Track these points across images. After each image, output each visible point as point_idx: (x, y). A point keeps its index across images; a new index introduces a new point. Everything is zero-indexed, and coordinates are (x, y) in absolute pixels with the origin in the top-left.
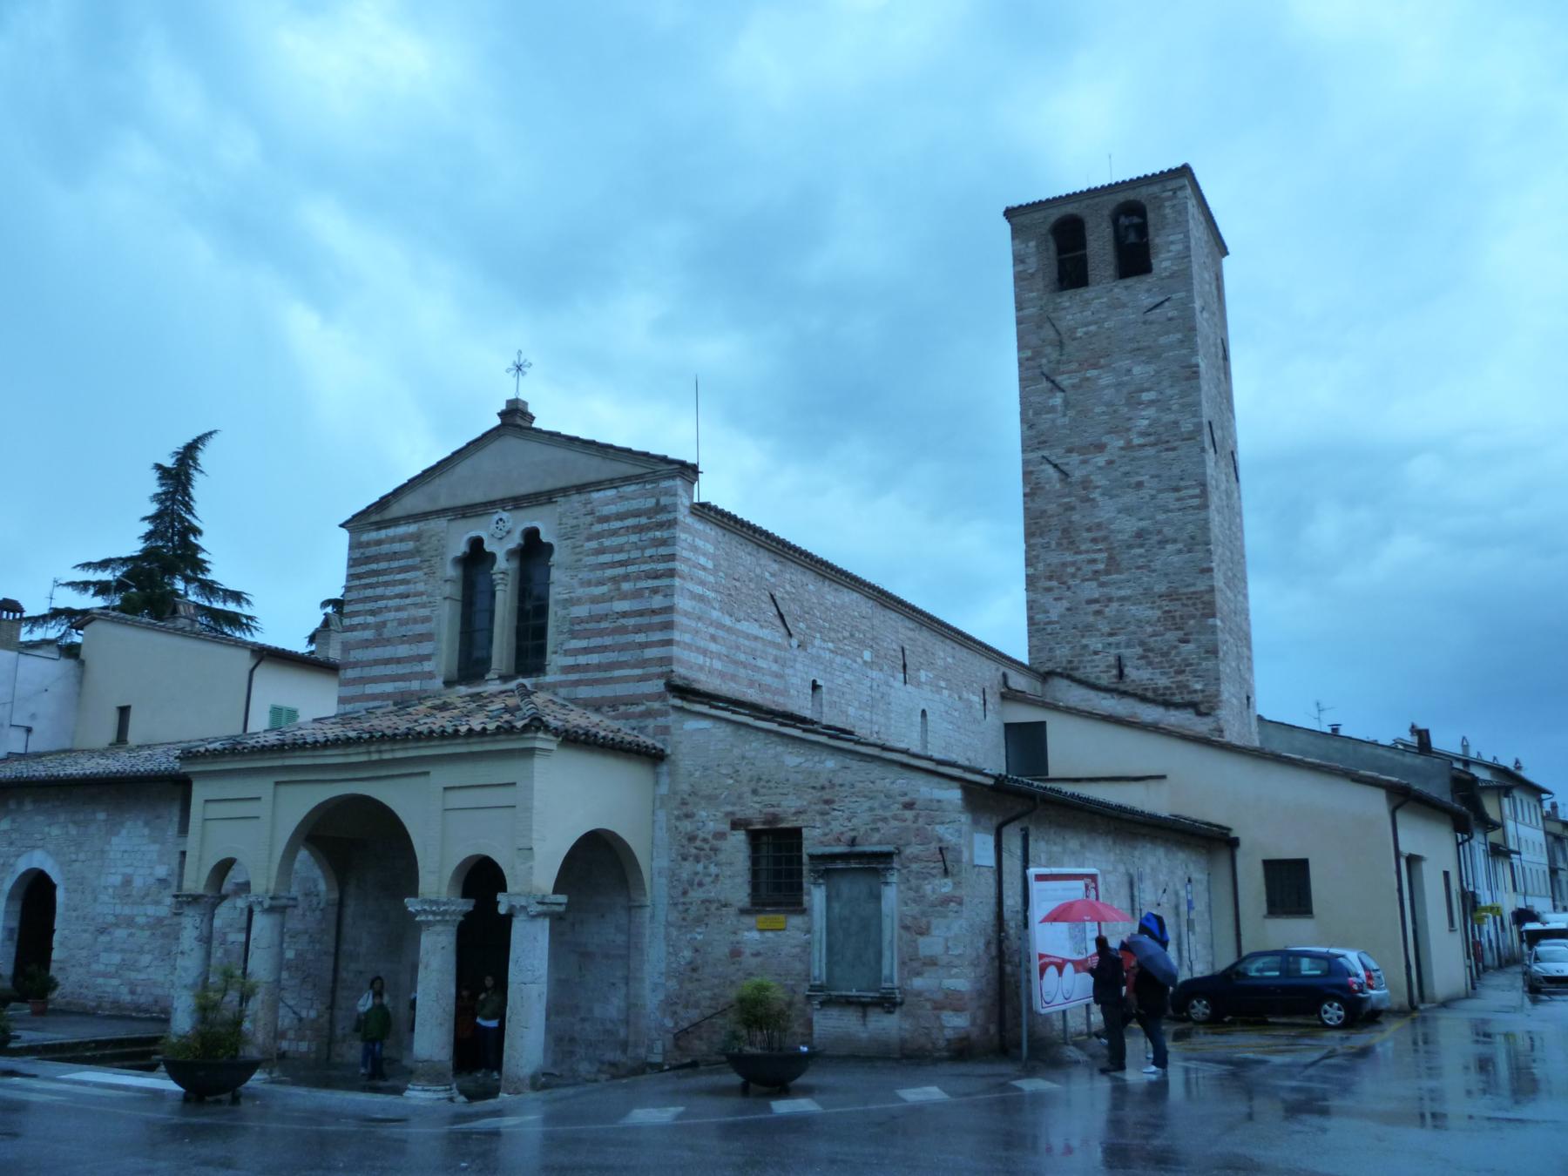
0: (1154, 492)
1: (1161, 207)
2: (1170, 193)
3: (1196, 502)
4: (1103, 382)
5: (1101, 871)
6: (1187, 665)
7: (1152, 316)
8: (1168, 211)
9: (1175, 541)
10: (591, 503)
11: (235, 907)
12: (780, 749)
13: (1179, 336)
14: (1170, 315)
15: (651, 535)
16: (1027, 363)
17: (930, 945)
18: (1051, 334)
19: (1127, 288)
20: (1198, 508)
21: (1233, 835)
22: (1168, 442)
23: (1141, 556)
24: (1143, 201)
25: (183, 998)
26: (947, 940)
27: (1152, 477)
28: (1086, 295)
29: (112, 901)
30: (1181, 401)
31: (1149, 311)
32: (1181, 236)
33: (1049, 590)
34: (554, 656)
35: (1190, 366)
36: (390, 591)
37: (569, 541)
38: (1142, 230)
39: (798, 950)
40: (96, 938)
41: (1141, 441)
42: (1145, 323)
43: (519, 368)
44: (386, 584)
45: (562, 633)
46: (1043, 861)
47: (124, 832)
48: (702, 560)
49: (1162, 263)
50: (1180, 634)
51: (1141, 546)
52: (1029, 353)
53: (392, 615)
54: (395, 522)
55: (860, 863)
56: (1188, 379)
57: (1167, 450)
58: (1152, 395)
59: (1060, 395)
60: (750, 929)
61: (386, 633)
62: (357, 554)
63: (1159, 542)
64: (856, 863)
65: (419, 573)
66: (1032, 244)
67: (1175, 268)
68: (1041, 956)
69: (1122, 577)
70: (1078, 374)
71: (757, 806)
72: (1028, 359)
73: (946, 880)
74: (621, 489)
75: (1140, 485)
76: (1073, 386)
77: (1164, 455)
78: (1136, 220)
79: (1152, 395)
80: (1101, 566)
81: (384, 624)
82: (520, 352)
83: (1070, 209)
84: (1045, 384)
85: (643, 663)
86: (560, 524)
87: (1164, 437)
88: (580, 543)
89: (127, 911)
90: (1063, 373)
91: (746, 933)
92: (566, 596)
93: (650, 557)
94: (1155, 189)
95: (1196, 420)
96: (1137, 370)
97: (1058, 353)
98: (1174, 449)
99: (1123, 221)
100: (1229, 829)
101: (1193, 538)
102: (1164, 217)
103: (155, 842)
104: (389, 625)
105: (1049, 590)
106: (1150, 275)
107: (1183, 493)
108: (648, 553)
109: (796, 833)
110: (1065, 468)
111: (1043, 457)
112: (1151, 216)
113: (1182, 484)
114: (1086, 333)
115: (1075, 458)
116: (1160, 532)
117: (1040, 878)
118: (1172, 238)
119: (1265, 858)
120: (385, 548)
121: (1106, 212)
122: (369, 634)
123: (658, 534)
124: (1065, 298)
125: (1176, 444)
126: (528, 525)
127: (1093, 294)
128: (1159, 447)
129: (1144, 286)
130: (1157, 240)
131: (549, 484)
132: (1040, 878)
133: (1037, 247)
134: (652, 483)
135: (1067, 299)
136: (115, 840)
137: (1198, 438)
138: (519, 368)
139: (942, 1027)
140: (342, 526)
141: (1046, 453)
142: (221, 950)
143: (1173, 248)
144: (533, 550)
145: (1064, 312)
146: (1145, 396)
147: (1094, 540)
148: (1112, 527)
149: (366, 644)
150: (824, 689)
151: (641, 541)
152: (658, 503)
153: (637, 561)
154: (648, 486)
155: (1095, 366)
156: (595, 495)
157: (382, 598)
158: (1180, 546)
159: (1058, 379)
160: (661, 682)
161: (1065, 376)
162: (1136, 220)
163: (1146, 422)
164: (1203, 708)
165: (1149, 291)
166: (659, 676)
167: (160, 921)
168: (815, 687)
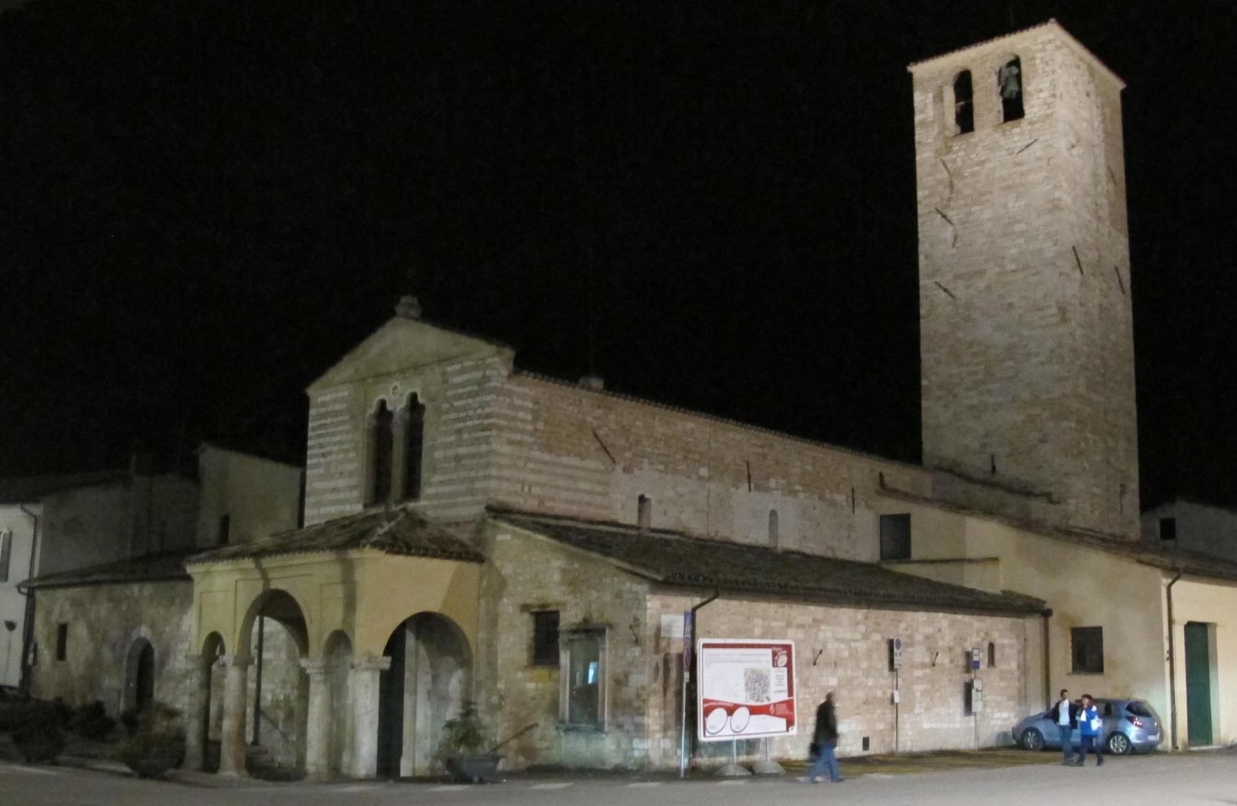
1: (1033, 58)
5: (795, 642)
8: (1038, 62)
9: (1037, 354)
13: (1044, 174)
21: (1047, 606)
28: (973, 140)
33: (939, 398)
41: (1013, 267)
46: (757, 631)
48: (521, 415)
59: (950, 228)
68: (705, 701)
80: (980, 377)
90: (953, 209)
97: (949, 192)
98: (1038, 273)
100: (1044, 602)
102: (1034, 66)
105: (939, 398)
106: (1022, 121)
109: (556, 613)
110: (953, 292)
111: (936, 283)
115: (960, 284)
117: (706, 646)
118: (1041, 86)
119: (1074, 626)
122: (322, 471)
124: (955, 144)
127: (977, 139)
132: (706, 646)
141: (938, 280)
143: (1041, 95)
144: (414, 406)
145: (954, 156)
147: (974, 355)
150: (653, 502)
155: (981, 204)
159: (950, 214)
161: (955, 212)
164: (1055, 497)
168: (642, 499)
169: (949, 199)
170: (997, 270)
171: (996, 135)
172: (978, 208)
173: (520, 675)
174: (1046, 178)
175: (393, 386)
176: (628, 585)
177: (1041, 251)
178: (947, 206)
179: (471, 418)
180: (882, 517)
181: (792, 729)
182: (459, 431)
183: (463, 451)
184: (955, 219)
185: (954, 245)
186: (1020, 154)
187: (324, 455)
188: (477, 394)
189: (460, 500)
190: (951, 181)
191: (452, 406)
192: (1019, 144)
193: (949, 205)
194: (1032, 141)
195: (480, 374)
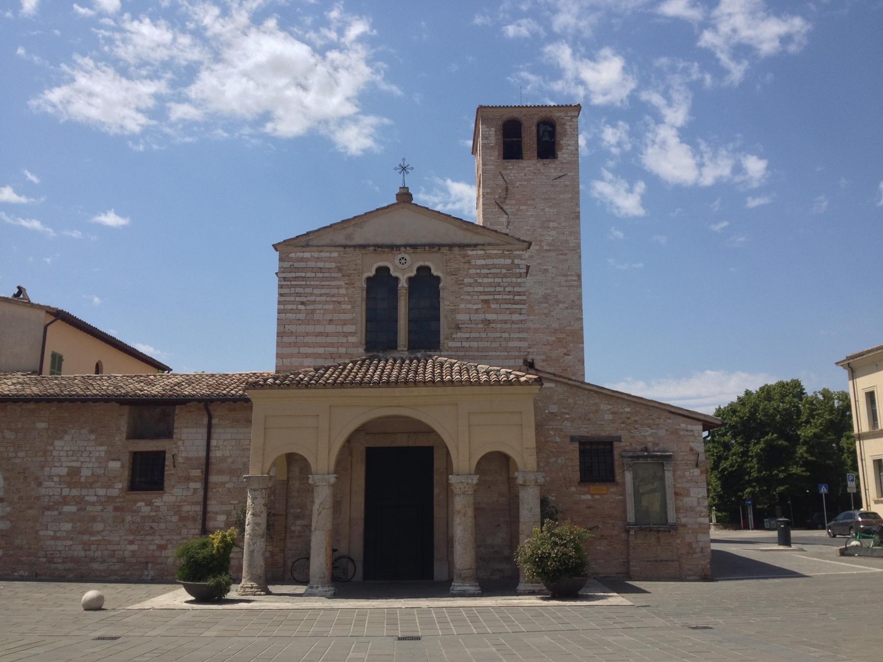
0: (554, 276)
1: (564, 124)
2: (569, 118)
3: (576, 283)
4: (528, 213)
6: (568, 367)
7: (557, 182)
9: (564, 302)
10: (468, 256)
11: (188, 488)
12: (597, 401)
13: (570, 195)
14: (566, 183)
15: (509, 280)
16: (487, 196)
17: (689, 501)
18: (501, 182)
19: (544, 164)
20: (576, 286)
22: (562, 250)
23: (546, 308)
24: (555, 119)
25: (258, 543)
26: (698, 499)
27: (553, 267)
28: (521, 165)
29: (58, 486)
30: (570, 230)
31: (556, 179)
32: (574, 142)
34: (446, 341)
35: (575, 213)
36: (316, 291)
37: (452, 277)
38: (552, 134)
39: (615, 504)
40: (43, 513)
41: (548, 248)
42: (552, 186)
43: (404, 169)
44: (316, 287)
45: (451, 328)
47: (67, 437)
49: (562, 155)
50: (565, 351)
51: (546, 303)
52: (489, 190)
53: (320, 306)
54: (320, 247)
55: (653, 460)
56: (573, 219)
57: (562, 254)
58: (555, 224)
60: (585, 494)
61: (316, 317)
62: (287, 265)
63: (556, 302)
64: (651, 460)
65: (342, 283)
66: (493, 129)
67: (570, 159)
69: (536, 318)
70: (515, 207)
71: (586, 430)
72: (488, 193)
73: (696, 470)
74: (488, 252)
75: (546, 270)
76: (512, 212)
77: (560, 257)
78: (549, 129)
79: (555, 224)
81: (313, 311)
82: (404, 159)
83: (515, 114)
84: (497, 209)
85: (506, 349)
86: (446, 266)
87: (560, 248)
88: (461, 278)
89: (75, 492)
91: (582, 496)
92: (452, 308)
93: (509, 292)
94: (562, 114)
95: (576, 241)
96: (547, 210)
97: (505, 193)
98: (565, 254)
99: (542, 128)
101: (573, 301)
103: (101, 445)
104: (318, 312)
107: (569, 278)
108: (508, 289)
112: (558, 128)
113: (569, 273)
114: (520, 185)
116: (556, 296)
118: (569, 142)
120: (312, 264)
121: (535, 121)
122: (301, 316)
123: (514, 280)
124: (509, 164)
125: (566, 252)
126: (421, 263)
127: (525, 165)
128: (557, 253)
129: (554, 166)
130: (561, 142)
131: (437, 241)
133: (496, 131)
134: (508, 251)
135: (511, 164)
136: (57, 443)
137: (578, 251)
138: (404, 169)
139: (697, 542)
140: (275, 247)
142: (177, 517)
143: (569, 148)
145: (509, 172)
146: (551, 224)
148: (531, 291)
149: (300, 322)
151: (502, 282)
152: (513, 263)
153: (501, 293)
154: (505, 252)
156: (470, 253)
157: (311, 294)
158: (567, 305)
159: (505, 207)
160: (521, 361)
162: (549, 129)
163: (551, 238)
165: (555, 168)
166: (518, 357)
167: (110, 499)
169: (505, 198)
170: (537, 247)
171: (539, 165)
172: (525, 207)
173: (573, 489)
174: (570, 198)
175: (400, 256)
176: (683, 426)
177: (567, 241)
178: (503, 202)
179: (499, 293)
180: (866, 393)
181: (265, 509)
182: (486, 302)
183: (490, 317)
184: (508, 211)
185: (507, 227)
186: (555, 180)
187: (303, 303)
188: (505, 276)
189: (490, 354)
190: (507, 187)
191: (476, 281)
192: (554, 174)
193: (505, 202)
194: (562, 174)
195: (508, 261)
